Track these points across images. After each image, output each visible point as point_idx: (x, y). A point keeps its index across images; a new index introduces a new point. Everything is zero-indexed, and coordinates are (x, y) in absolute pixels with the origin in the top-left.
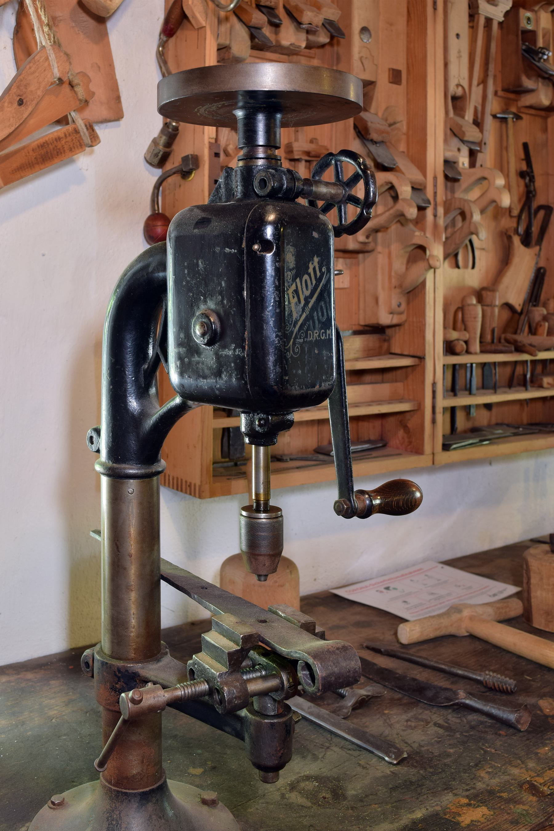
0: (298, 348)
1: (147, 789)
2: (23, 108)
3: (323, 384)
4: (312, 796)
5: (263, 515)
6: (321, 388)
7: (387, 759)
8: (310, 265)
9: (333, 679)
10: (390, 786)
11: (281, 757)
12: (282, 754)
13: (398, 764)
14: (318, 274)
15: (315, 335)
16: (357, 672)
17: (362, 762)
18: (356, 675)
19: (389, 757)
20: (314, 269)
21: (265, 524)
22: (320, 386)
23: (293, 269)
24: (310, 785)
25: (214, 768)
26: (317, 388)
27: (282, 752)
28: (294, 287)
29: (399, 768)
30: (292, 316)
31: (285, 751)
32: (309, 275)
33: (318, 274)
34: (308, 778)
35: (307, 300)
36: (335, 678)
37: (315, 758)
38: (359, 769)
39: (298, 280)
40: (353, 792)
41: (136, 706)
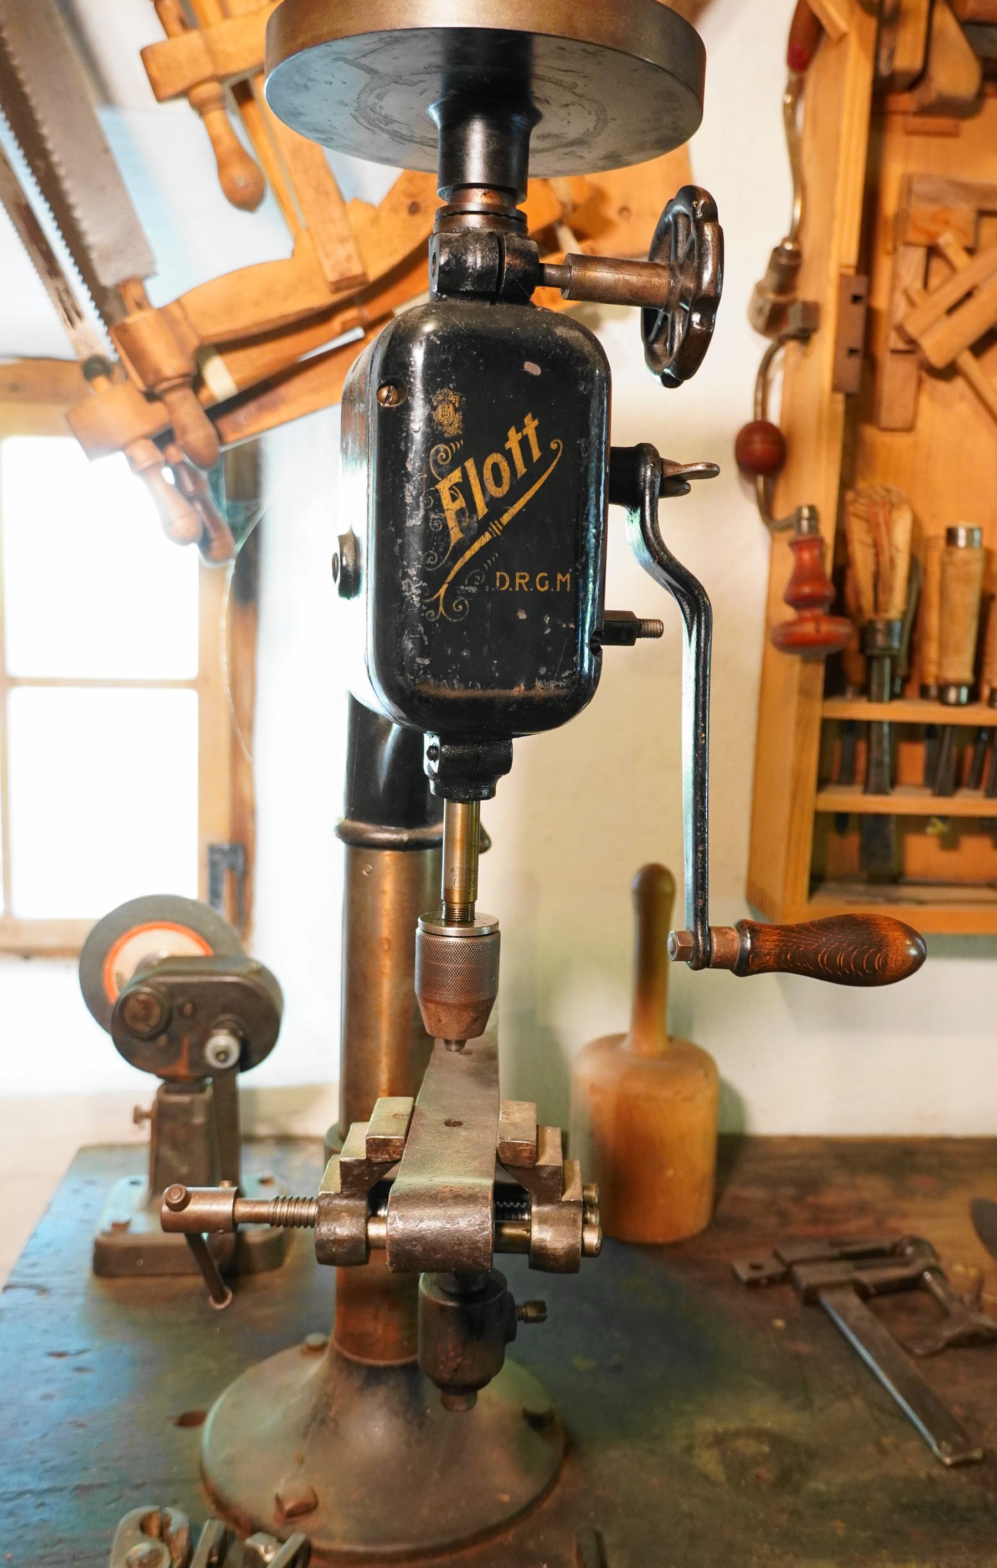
0: (462, 603)
1: (381, 1363)
2: (418, 219)
3: (538, 684)
4: (738, 1469)
5: (452, 930)
6: (532, 693)
7: (935, 1449)
8: (512, 433)
9: (419, 1248)
10: (904, 1500)
11: (456, 1370)
12: (459, 1365)
13: (955, 1466)
14: (536, 454)
15: (518, 581)
16: (478, 1248)
17: (887, 1441)
18: (477, 1253)
19: (939, 1447)
20: (524, 443)
21: (455, 946)
22: (530, 686)
23: (455, 439)
24: (748, 1447)
25: (618, 1368)
26: (519, 690)
27: (459, 1360)
28: (456, 476)
29: (954, 1473)
30: (448, 535)
31: (467, 1362)
32: (508, 455)
33: (536, 454)
34: (760, 1435)
35: (496, 507)
36: (424, 1250)
37: (807, 1405)
38: (870, 1449)
39: (470, 464)
40: (822, 1487)
41: (173, 1213)
